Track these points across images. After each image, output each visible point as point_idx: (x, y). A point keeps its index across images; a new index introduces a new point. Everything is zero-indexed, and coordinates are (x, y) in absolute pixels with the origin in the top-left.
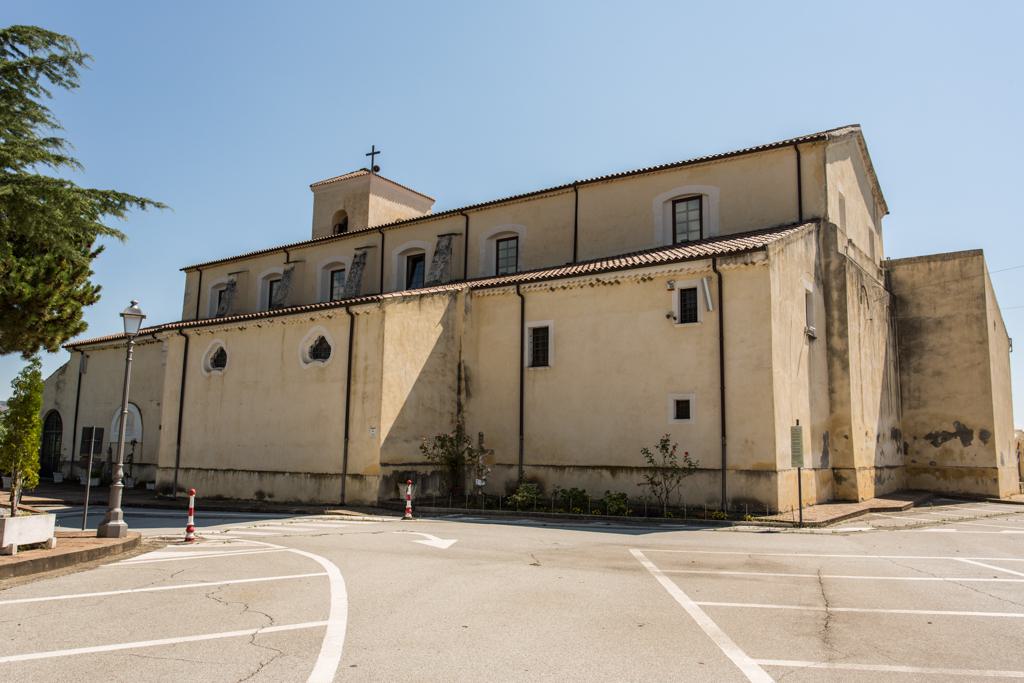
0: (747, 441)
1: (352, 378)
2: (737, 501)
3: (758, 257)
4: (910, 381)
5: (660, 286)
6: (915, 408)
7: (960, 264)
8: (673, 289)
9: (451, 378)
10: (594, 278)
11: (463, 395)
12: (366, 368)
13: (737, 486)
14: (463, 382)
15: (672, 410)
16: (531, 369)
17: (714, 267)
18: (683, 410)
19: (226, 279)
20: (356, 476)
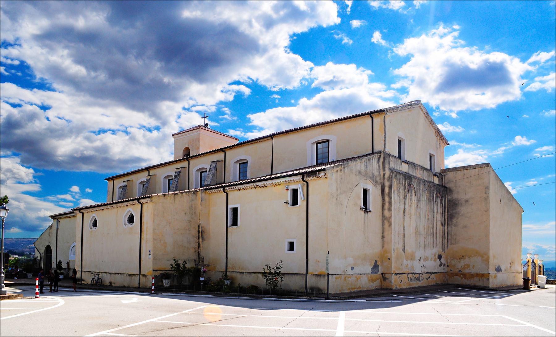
0: (316, 261)
1: (142, 232)
2: (312, 289)
3: (322, 174)
4: (452, 231)
5: (282, 188)
6: (454, 244)
7: (478, 171)
8: (288, 190)
9: (194, 232)
10: (255, 184)
11: (201, 239)
12: (147, 228)
13: (312, 281)
14: (201, 234)
15: (287, 246)
16: (231, 227)
17: (303, 179)
18: (291, 246)
19: (123, 184)
20: (144, 275)
